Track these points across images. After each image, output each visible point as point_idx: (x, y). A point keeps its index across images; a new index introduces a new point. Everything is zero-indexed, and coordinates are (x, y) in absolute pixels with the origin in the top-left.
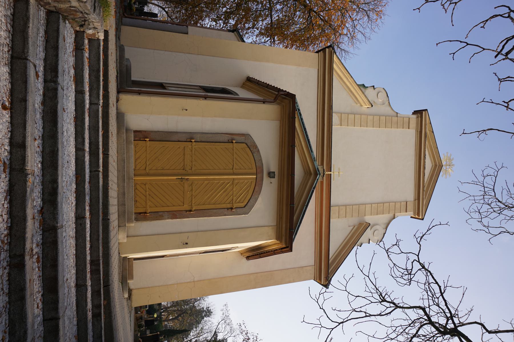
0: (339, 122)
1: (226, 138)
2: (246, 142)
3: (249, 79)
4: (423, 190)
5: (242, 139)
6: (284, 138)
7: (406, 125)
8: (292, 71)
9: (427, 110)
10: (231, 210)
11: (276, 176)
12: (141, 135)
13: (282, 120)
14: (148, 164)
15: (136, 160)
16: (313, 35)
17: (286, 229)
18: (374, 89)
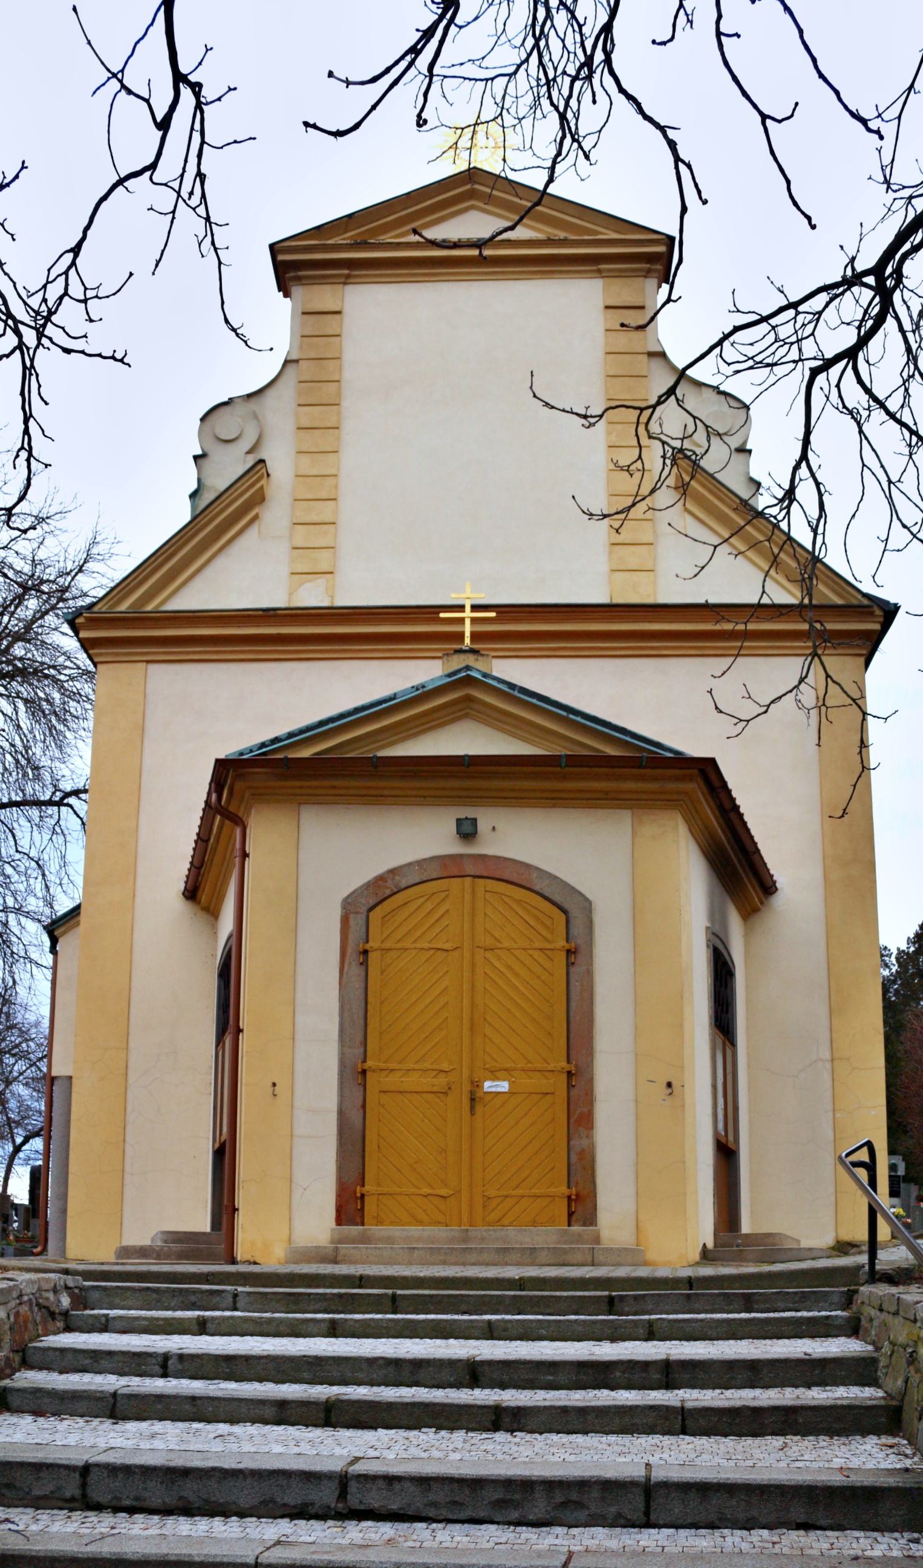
0: (321, 581)
1: (355, 970)
2: (364, 909)
3: (191, 893)
4: (563, 243)
6: (352, 792)
10: (576, 954)
12: (350, 1207)
14: (430, 1191)
15: (420, 1223)
16: (24, 1309)
17: (643, 778)
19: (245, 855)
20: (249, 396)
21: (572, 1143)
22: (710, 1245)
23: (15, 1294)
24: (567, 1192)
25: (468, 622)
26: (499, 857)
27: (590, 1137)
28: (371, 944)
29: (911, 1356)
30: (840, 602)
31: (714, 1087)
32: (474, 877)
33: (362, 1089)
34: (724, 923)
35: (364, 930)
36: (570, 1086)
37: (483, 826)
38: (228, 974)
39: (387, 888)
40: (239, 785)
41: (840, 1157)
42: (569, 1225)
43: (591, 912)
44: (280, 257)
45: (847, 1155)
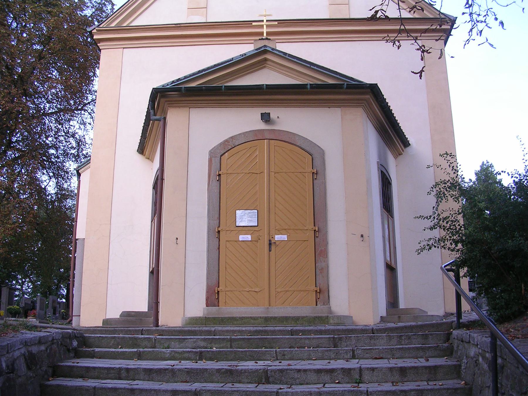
1: (215, 184)
3: (141, 150)
5: (216, 161)
10: (317, 174)
12: (213, 297)
13: (191, 105)
22: (384, 314)
23: (50, 339)
25: (265, 26)
29: (476, 362)
30: (431, 16)
31: (384, 237)
34: (386, 159)
38: (158, 185)
39: (229, 145)
40: (163, 100)
41: (441, 268)
45: (445, 266)
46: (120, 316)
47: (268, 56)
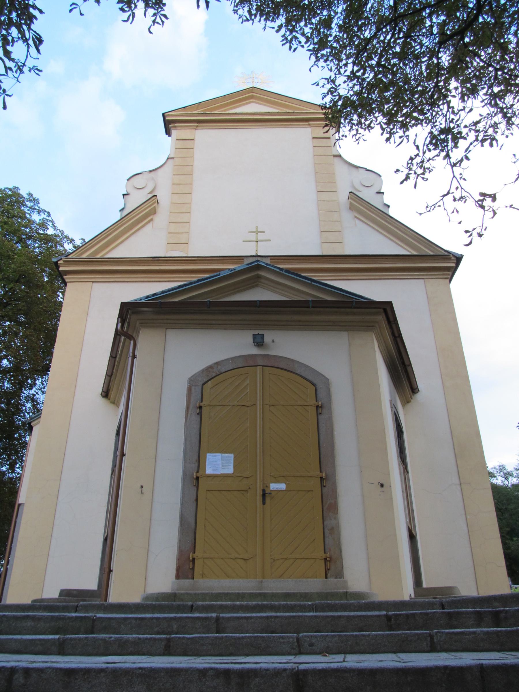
1: (195, 418)
2: (200, 384)
3: (106, 394)
7: (189, 144)
8: (87, 320)
9: (163, 114)
10: (321, 408)
11: (261, 332)
12: (186, 567)
14: (237, 556)
17: (354, 314)
18: (127, 194)
19: (134, 357)
20: (151, 171)
21: (325, 523)
24: (324, 556)
26: (277, 356)
27: (336, 518)
28: (204, 403)
32: (263, 366)
33: (196, 489)
35: (200, 395)
36: (322, 486)
37: (268, 339)
42: (326, 577)
43: (329, 385)
44: (167, 119)
46: (60, 595)
47: (263, 273)
